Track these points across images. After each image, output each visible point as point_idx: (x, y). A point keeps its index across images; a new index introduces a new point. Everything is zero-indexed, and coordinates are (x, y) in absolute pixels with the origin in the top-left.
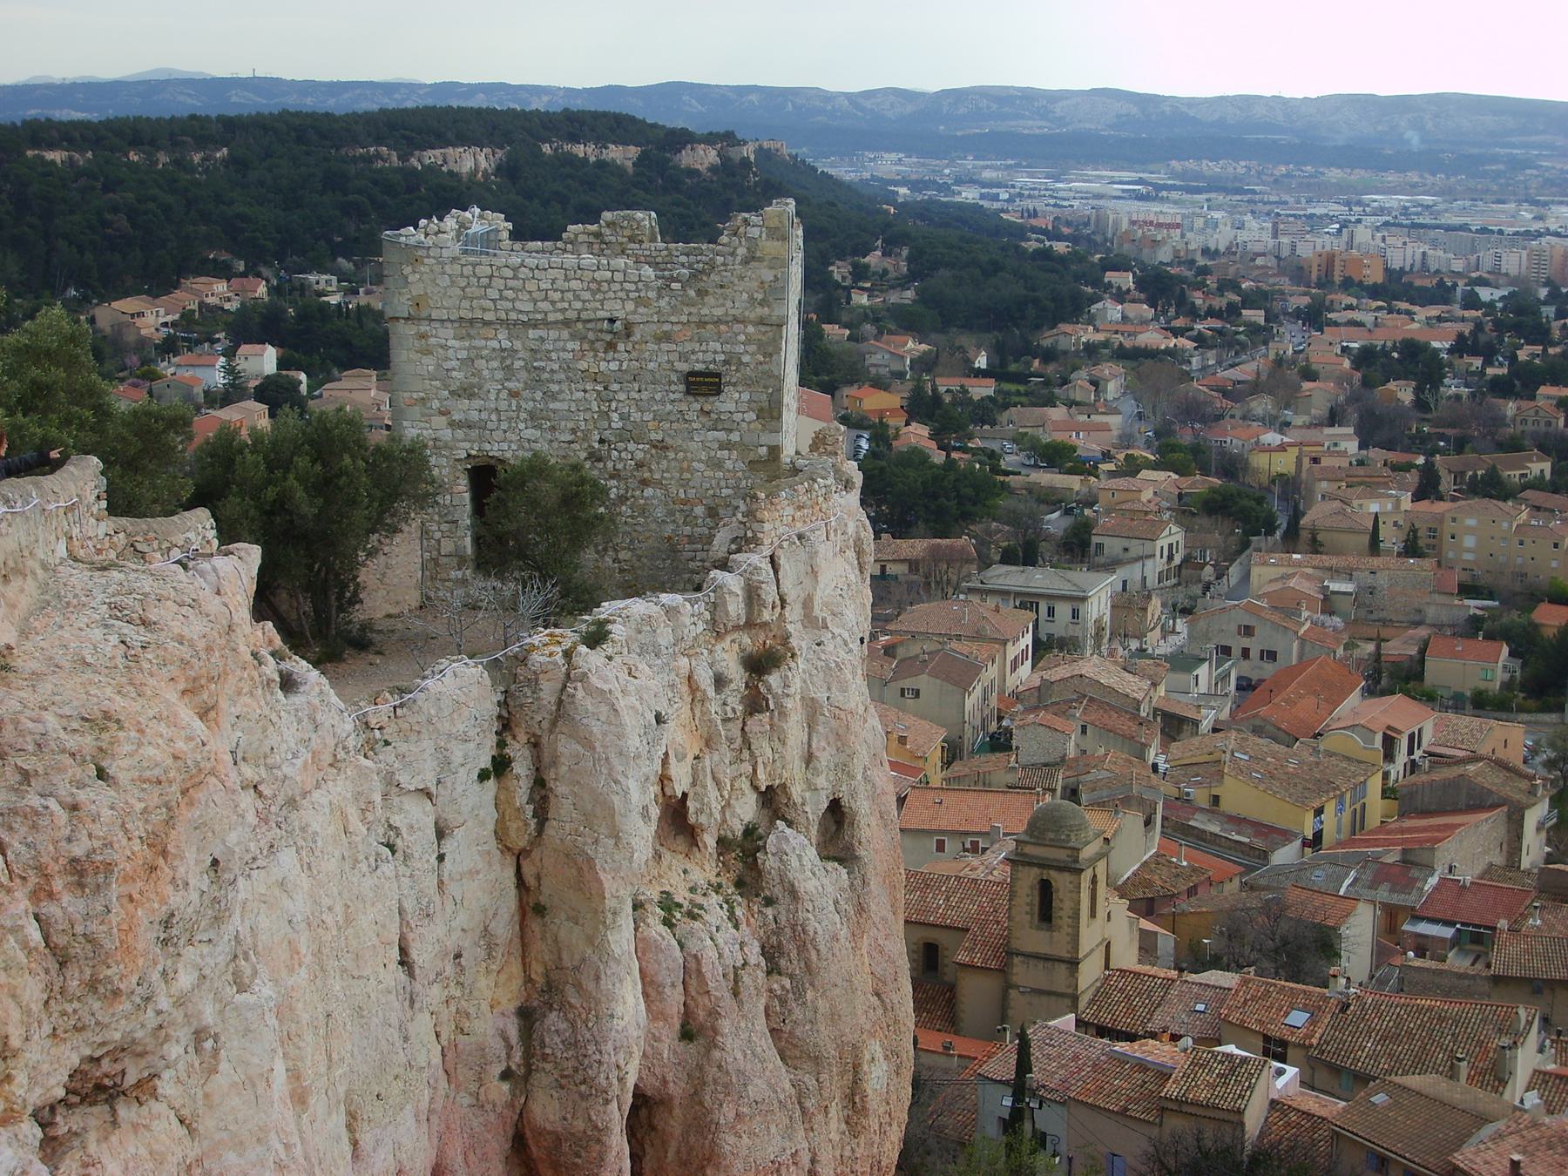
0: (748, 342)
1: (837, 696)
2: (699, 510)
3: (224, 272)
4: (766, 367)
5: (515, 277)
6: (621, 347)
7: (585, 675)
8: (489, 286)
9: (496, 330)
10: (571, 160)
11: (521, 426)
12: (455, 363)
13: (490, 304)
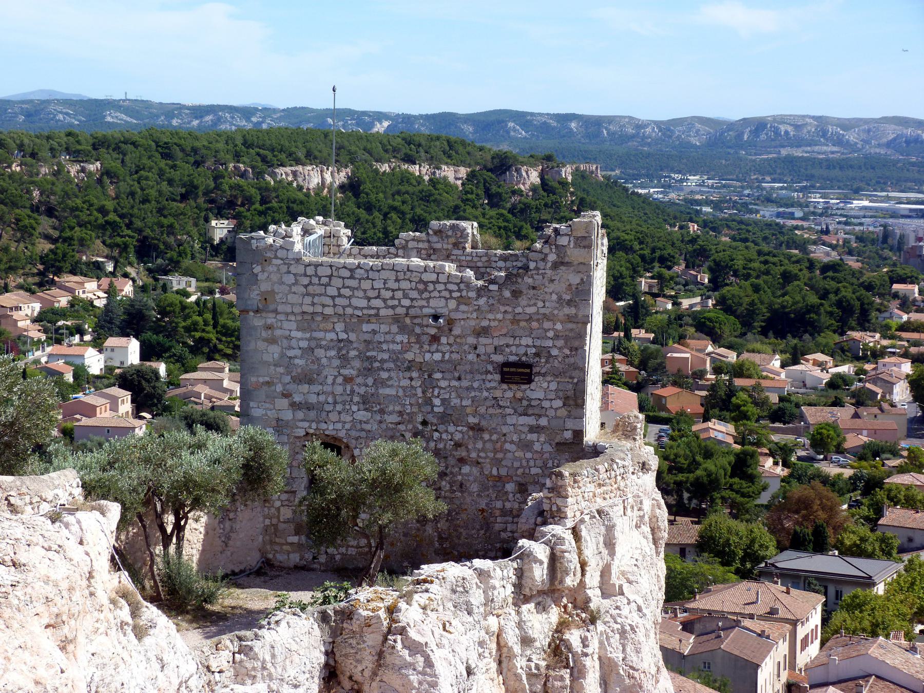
0: (557, 337)
1: (633, 658)
2: (510, 487)
3: (96, 271)
4: (572, 360)
5: (352, 277)
6: (444, 340)
7: (404, 628)
8: (329, 284)
9: (334, 323)
10: (406, 178)
11: (355, 408)
12: (298, 352)
13: (329, 301)
